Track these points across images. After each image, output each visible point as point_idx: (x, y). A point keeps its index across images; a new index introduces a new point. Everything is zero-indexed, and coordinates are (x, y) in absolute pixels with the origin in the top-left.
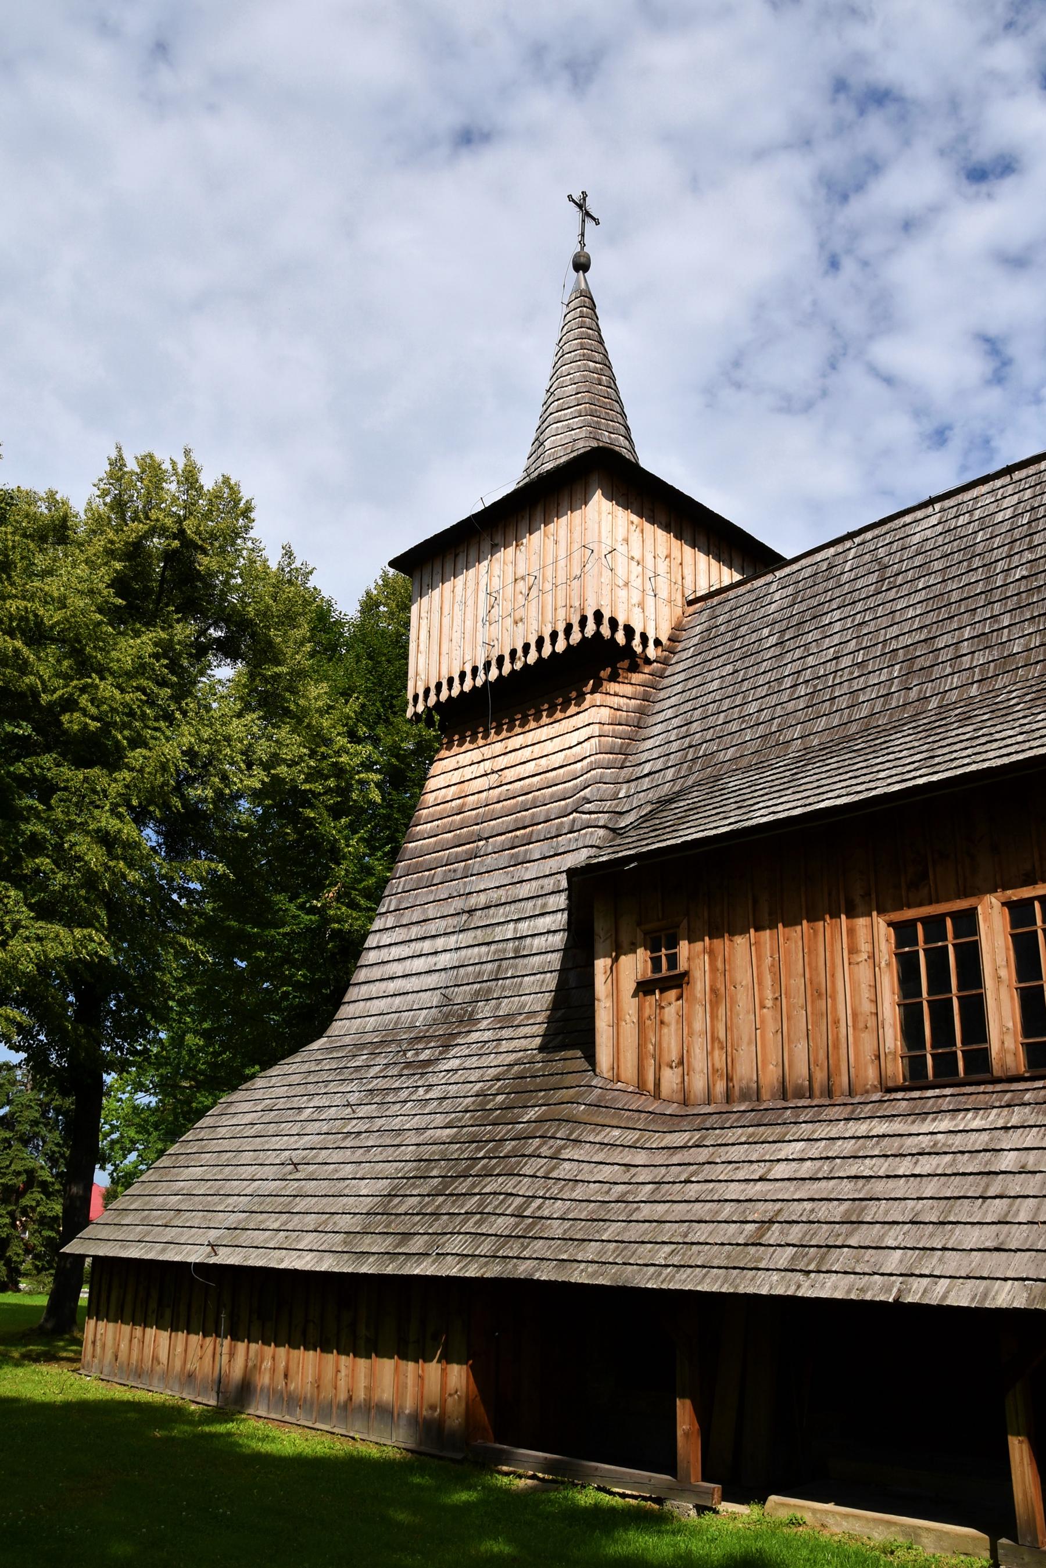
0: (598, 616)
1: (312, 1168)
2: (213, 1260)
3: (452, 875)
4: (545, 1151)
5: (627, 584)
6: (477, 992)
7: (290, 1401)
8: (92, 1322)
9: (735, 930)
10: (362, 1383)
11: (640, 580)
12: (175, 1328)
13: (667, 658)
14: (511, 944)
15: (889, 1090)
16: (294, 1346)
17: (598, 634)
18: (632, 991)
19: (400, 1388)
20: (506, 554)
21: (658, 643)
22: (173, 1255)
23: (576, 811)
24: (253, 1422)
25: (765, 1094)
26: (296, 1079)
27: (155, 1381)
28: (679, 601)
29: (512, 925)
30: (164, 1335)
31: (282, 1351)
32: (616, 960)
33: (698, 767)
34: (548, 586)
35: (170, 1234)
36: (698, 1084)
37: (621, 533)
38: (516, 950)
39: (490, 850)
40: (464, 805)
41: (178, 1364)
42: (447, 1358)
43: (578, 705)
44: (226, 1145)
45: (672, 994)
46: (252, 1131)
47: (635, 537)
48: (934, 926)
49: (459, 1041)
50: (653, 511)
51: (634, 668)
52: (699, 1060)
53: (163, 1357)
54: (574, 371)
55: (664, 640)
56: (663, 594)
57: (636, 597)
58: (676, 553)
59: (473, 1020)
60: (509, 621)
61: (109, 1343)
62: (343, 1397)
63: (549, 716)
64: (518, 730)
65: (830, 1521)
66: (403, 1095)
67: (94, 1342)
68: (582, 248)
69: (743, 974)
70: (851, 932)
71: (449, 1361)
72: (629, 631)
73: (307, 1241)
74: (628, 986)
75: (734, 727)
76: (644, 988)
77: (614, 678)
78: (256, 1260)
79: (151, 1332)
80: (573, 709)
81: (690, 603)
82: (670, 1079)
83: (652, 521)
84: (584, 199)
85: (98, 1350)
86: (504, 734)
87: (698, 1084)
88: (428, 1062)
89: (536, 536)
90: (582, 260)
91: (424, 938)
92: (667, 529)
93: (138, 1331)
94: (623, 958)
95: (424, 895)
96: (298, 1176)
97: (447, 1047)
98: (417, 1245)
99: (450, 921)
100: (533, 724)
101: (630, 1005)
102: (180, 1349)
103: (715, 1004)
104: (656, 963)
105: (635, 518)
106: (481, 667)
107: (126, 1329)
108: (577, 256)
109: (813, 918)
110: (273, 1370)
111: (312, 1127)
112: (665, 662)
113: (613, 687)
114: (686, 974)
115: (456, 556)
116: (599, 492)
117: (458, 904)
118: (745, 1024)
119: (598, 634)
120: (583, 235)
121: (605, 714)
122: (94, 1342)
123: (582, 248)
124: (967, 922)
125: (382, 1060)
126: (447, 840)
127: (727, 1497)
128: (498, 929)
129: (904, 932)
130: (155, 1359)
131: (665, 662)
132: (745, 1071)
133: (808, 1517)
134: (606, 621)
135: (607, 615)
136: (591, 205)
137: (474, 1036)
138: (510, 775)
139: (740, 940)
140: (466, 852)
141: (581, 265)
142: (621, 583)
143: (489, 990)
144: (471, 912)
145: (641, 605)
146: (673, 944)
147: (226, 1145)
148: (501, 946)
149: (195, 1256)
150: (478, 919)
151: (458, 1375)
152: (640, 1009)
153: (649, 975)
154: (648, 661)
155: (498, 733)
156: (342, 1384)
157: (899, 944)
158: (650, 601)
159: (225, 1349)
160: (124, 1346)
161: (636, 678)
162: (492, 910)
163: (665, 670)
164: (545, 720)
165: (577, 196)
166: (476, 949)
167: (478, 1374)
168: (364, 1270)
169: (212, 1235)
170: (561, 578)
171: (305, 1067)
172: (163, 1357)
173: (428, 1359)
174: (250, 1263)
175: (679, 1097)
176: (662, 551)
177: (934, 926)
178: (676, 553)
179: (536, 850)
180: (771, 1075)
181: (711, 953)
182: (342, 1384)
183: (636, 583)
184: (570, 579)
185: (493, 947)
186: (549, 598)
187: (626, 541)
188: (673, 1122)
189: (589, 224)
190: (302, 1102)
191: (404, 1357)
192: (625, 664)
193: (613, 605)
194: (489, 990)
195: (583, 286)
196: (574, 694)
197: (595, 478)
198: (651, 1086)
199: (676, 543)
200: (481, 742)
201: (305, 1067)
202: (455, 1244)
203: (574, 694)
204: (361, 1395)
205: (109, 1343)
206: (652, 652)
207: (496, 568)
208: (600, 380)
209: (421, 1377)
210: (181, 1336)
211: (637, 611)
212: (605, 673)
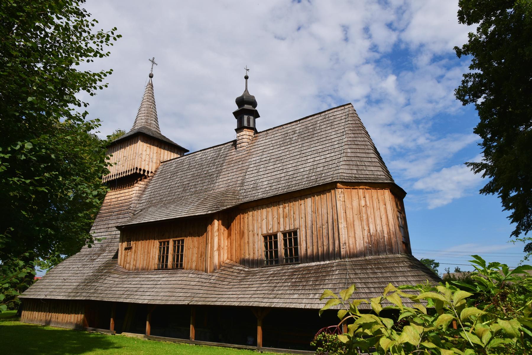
0: (137, 168)
1: (68, 280)
2: (46, 298)
3: (106, 219)
4: (104, 278)
5: (145, 160)
6: (107, 245)
7: (58, 323)
8: (23, 311)
9: (139, 240)
10: (69, 318)
11: (148, 159)
12: (39, 311)
13: (153, 176)
14: (114, 236)
15: (155, 270)
16: (59, 313)
17: (136, 172)
18: (481, 189)
19: (74, 319)
20: (123, 150)
21: (151, 172)
22: (39, 297)
23: (129, 209)
24: (50, 327)
25: (140, 270)
26: (71, 261)
27: (35, 322)
28: (159, 162)
29: (115, 232)
30: (37, 313)
31: (57, 314)
32: (122, 243)
33: (149, 203)
34: (129, 160)
35: (39, 293)
36: (131, 267)
37: (144, 149)
38: (115, 237)
39: (114, 215)
40: (111, 204)
41: (39, 318)
42: (81, 314)
43: (133, 186)
44: (54, 275)
45: (129, 250)
46: (60, 272)
47: (148, 149)
48: (179, 241)
49: (101, 255)
50: (154, 143)
51: (146, 178)
52: (132, 263)
53: (37, 317)
54: (146, 105)
55: (154, 172)
56: (154, 161)
57: (147, 162)
58: (159, 152)
59: (105, 251)
60: (122, 165)
61: (27, 315)
62: (66, 321)
63: (128, 187)
64: (122, 189)
65: (128, 335)
66: (88, 266)
67: (23, 315)
68: (152, 72)
69: (139, 248)
70: (154, 243)
71: (82, 314)
72: (144, 171)
73: (63, 294)
74: (124, 249)
75: (157, 195)
76: (126, 249)
77: (140, 180)
78: (53, 298)
79: (35, 312)
80: (132, 187)
81: (161, 163)
82: (128, 265)
83: (153, 145)
84: (154, 59)
85: (24, 317)
86: (120, 189)
87: (131, 267)
88: (95, 259)
89: (128, 147)
90: (151, 75)
91: (100, 232)
92: (157, 146)
93: (32, 312)
94: (123, 243)
95: (101, 223)
96: (65, 282)
97: (99, 256)
98: (78, 294)
99: (105, 229)
100: (125, 188)
101: (124, 252)
102: (40, 315)
103: (135, 253)
104: (128, 244)
105: (149, 145)
106: (116, 175)
107: (30, 312)
108: (150, 74)
109: (149, 240)
110: (55, 318)
111: (71, 272)
112: (153, 177)
113: (140, 182)
114: (131, 247)
115: (114, 148)
116: (140, 141)
117: (106, 226)
118: (139, 258)
119: (136, 172)
120: (152, 68)
121: (138, 188)
122: (23, 315)
123: (152, 72)
124: (168, 242)
125: (87, 258)
126: (107, 211)
127: (117, 333)
128: (113, 232)
129: (160, 243)
130: (35, 318)
131: (153, 177)
132: (138, 265)
133: (126, 335)
134: (138, 169)
135: (139, 168)
136: (155, 61)
137: (104, 254)
138: (119, 199)
139: (139, 242)
140: (110, 215)
141: (151, 76)
142: (143, 160)
143: (109, 245)
144: (108, 228)
145: (148, 165)
146: (131, 242)
147: (54, 275)
148: (112, 236)
149: (43, 297)
150: (110, 230)
151: (83, 315)
152: (125, 253)
153: (127, 247)
154: (149, 177)
155: (119, 189)
156: (66, 319)
157: (160, 246)
158: (151, 163)
159: (48, 315)
160: (29, 316)
161: (146, 180)
162: (112, 228)
163: (152, 178)
164: (127, 188)
165: (151, 59)
166: (108, 236)
167: (85, 316)
168: (69, 299)
169: (46, 293)
170: (131, 159)
171: (74, 259)
172: (37, 317)
173: (79, 314)
174: (52, 298)
175: (128, 269)
176: (155, 152)
177: (164, 242)
178: (159, 152)
179: (121, 216)
180: (141, 267)
181: (135, 244)
182: (66, 319)
183: (147, 159)
184: (133, 159)
185: (111, 236)
186: (129, 162)
187: (146, 151)
188: (125, 273)
189: (155, 65)
190: (70, 266)
191: (75, 314)
192: (144, 177)
193: (141, 165)
194: (109, 245)
195: (150, 82)
196: (132, 183)
197: (139, 137)
198: (125, 267)
199: (159, 149)
200: (116, 190)
201: (74, 259)
202: (84, 294)
203: (132, 183)
204: (69, 321)
205: (27, 315)
206: (150, 175)
207: (121, 153)
208: (150, 107)
209: (78, 317)
210: (40, 313)
211: (147, 166)
212: (138, 179)
